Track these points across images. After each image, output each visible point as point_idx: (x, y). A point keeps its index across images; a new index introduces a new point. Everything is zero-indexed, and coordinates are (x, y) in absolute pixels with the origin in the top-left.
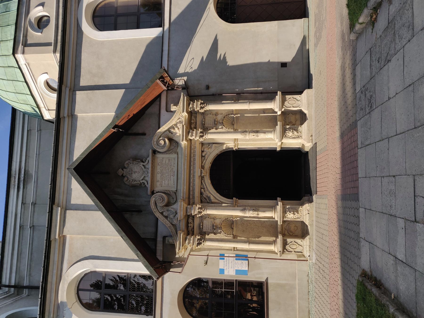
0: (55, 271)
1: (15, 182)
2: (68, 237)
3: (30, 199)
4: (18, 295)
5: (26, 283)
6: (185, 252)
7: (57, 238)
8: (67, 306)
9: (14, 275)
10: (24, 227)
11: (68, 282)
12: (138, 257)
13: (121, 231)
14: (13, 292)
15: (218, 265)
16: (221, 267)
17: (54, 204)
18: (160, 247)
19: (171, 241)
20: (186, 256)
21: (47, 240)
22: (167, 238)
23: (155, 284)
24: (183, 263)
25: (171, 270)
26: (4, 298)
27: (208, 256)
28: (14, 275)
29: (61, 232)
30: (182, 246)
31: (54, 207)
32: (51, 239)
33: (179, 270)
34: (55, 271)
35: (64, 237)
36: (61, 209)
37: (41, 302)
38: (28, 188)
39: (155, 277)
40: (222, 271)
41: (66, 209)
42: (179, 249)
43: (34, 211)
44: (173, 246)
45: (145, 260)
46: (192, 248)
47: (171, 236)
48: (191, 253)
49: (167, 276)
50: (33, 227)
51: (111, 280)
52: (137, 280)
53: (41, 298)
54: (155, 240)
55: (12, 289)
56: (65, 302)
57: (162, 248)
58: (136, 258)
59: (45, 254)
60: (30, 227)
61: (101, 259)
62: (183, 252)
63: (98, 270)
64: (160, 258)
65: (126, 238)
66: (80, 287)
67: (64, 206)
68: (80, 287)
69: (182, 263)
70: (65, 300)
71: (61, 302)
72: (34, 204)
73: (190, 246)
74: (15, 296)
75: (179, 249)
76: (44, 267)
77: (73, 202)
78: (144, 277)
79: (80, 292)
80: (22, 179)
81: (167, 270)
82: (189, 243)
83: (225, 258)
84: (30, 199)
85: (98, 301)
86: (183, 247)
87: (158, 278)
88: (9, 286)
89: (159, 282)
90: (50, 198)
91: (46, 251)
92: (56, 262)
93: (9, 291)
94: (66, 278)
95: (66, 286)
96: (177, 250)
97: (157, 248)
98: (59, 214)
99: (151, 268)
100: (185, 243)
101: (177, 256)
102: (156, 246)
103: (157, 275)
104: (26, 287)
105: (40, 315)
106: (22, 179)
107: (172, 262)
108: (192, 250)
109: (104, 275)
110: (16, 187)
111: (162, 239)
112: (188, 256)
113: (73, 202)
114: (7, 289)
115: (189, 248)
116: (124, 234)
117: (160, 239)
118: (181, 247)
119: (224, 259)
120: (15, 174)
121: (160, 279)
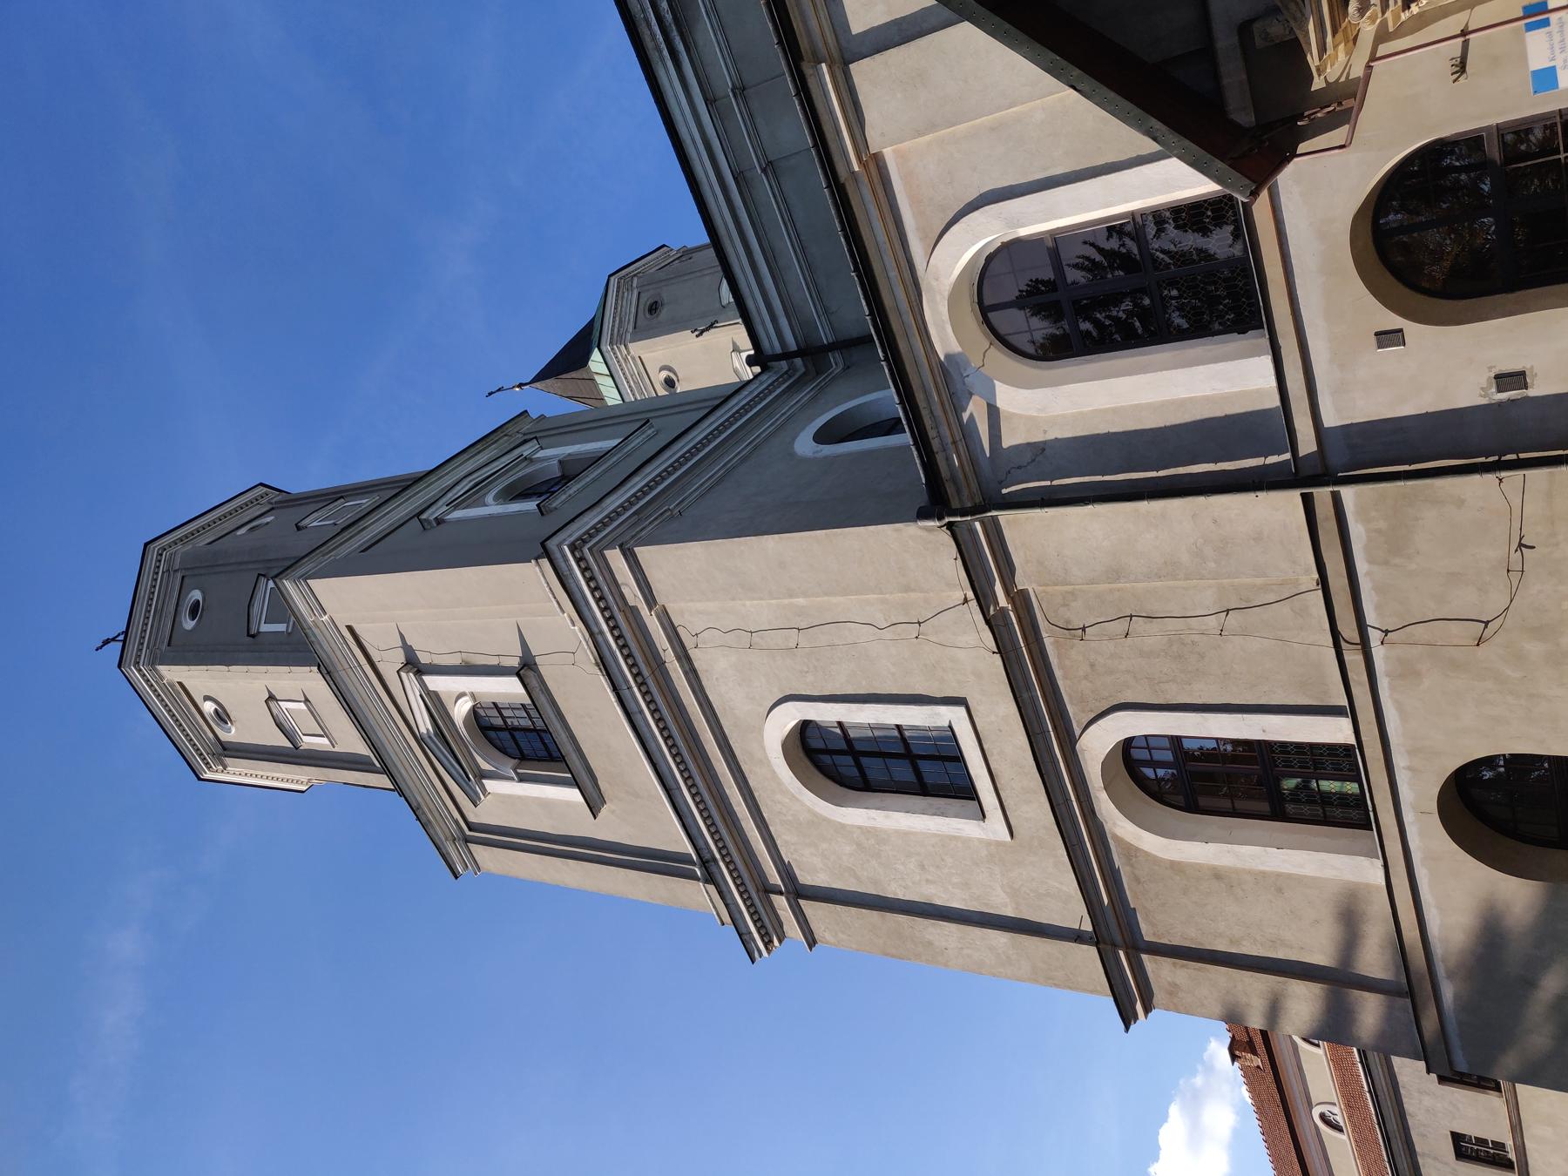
0: (893, 274)
1: (653, 36)
2: (888, 153)
3: (724, 79)
4: (818, 373)
5: (825, 336)
6: (1349, 54)
7: (856, 169)
8: (968, 363)
9: (784, 322)
10: (748, 174)
11: (946, 294)
12: (1155, 139)
13: (1064, 63)
14: (803, 370)
15: (1523, 57)
16: (1537, 62)
17: (801, 58)
18: (1233, 75)
19: (1276, 29)
20: (1357, 71)
21: (829, 186)
22: (1257, 26)
23: (1244, 230)
24: (1347, 104)
25: (1302, 148)
26: (784, 392)
27: (1464, 33)
28: (784, 322)
29: (862, 147)
30: (1334, 33)
31: (807, 69)
32: (842, 180)
33: (1338, 135)
34: (893, 274)
35: (878, 159)
36: (830, 67)
37: (890, 370)
38: (700, 43)
39: (1241, 193)
40: (1546, 79)
41: (846, 63)
42: (1322, 49)
43: (751, 116)
44: (1295, 50)
45: (1187, 143)
46: (1384, 24)
47: (1274, 11)
48: (1383, 50)
49: (1287, 178)
50: (770, 167)
51: (1076, 266)
52: (1172, 247)
53: (886, 359)
54: (1206, 53)
55: (798, 361)
56: (959, 354)
57: (1244, 77)
58: (1154, 147)
59: (843, 229)
60: (764, 170)
61: (1023, 195)
62: (1342, 57)
63: (1023, 232)
64: (1246, 118)
65: (1089, 83)
66: (987, 302)
67: (836, 54)
68: (987, 302)
69: (1343, 104)
70: (956, 348)
71: (947, 356)
72: (740, 90)
73: (1373, 19)
74: (814, 379)
75: (1322, 49)
76: (856, 269)
77: (857, 27)
78: (1190, 215)
79: (990, 315)
80: (669, 17)
81: (1283, 154)
82: (1362, 11)
83: (1554, 17)
84: (724, 79)
85: (1052, 339)
86: (1340, 35)
87: (1255, 194)
88: (787, 356)
89: (1261, 209)
90: (780, 43)
91: (841, 222)
92: (882, 237)
93: (792, 369)
94: (934, 283)
95: (944, 309)
96: (1313, 60)
97: (1225, 81)
98: (830, 86)
99: (1219, 164)
100: (1346, 14)
101: (1318, 84)
102: (1216, 77)
103: (1247, 182)
104: (832, 347)
105: (902, 403)
106: (669, 17)
107: (1301, 117)
108: (1382, 36)
109: (1050, 244)
110: (665, 52)
111: (1235, 40)
112: (1369, 67)
113: (857, 27)
114: (784, 365)
115: (1368, 29)
116: (1076, 72)
117: (1225, 41)
118: (1329, 39)
119: (1546, 23)
120: (643, 10)
121: (1264, 194)
